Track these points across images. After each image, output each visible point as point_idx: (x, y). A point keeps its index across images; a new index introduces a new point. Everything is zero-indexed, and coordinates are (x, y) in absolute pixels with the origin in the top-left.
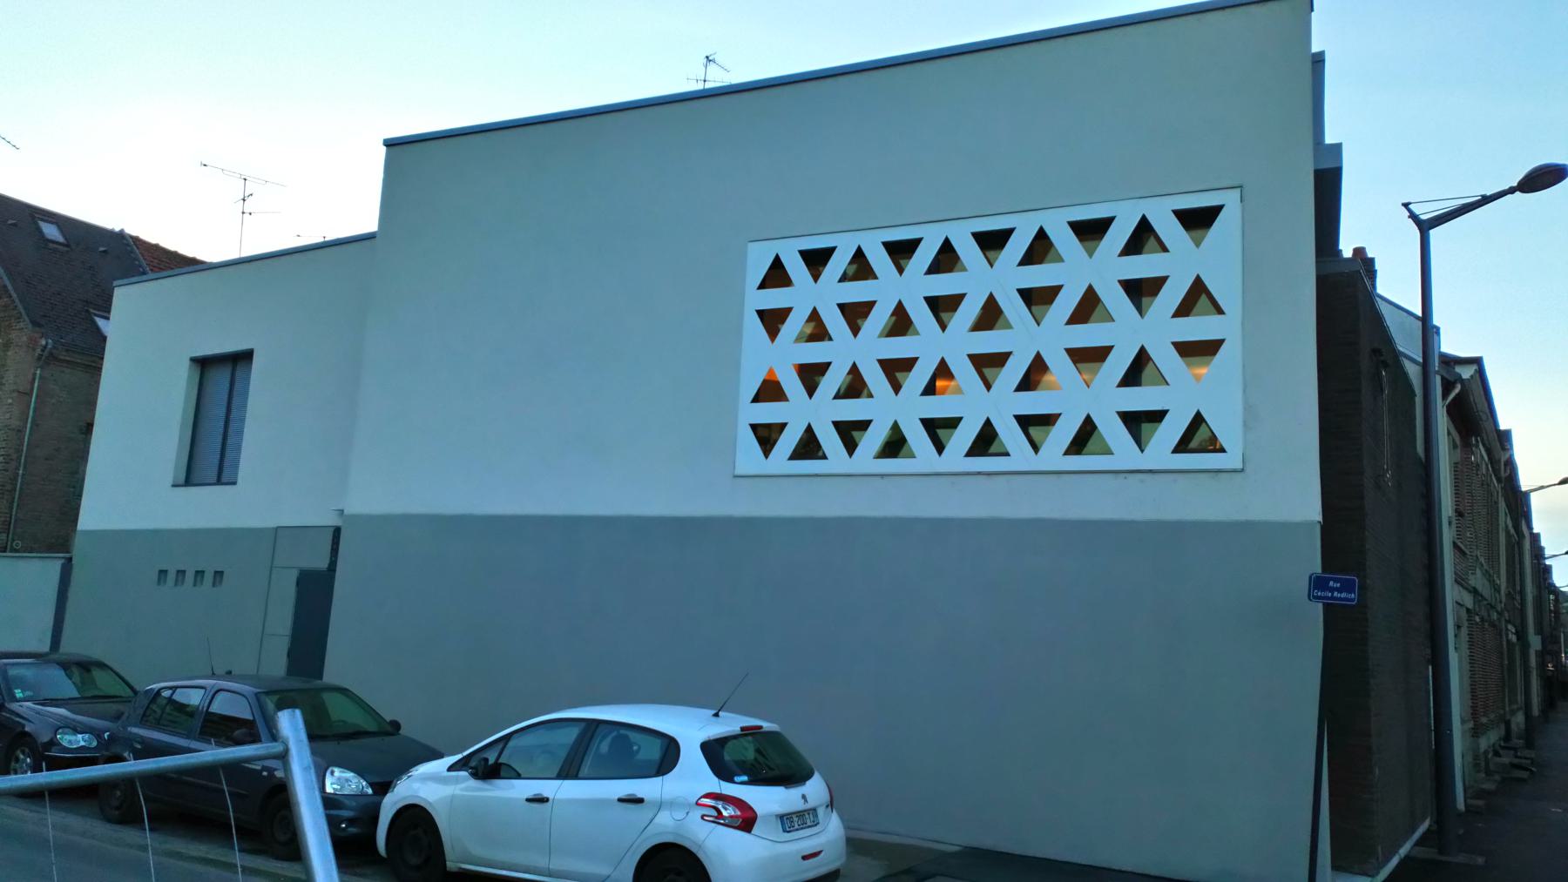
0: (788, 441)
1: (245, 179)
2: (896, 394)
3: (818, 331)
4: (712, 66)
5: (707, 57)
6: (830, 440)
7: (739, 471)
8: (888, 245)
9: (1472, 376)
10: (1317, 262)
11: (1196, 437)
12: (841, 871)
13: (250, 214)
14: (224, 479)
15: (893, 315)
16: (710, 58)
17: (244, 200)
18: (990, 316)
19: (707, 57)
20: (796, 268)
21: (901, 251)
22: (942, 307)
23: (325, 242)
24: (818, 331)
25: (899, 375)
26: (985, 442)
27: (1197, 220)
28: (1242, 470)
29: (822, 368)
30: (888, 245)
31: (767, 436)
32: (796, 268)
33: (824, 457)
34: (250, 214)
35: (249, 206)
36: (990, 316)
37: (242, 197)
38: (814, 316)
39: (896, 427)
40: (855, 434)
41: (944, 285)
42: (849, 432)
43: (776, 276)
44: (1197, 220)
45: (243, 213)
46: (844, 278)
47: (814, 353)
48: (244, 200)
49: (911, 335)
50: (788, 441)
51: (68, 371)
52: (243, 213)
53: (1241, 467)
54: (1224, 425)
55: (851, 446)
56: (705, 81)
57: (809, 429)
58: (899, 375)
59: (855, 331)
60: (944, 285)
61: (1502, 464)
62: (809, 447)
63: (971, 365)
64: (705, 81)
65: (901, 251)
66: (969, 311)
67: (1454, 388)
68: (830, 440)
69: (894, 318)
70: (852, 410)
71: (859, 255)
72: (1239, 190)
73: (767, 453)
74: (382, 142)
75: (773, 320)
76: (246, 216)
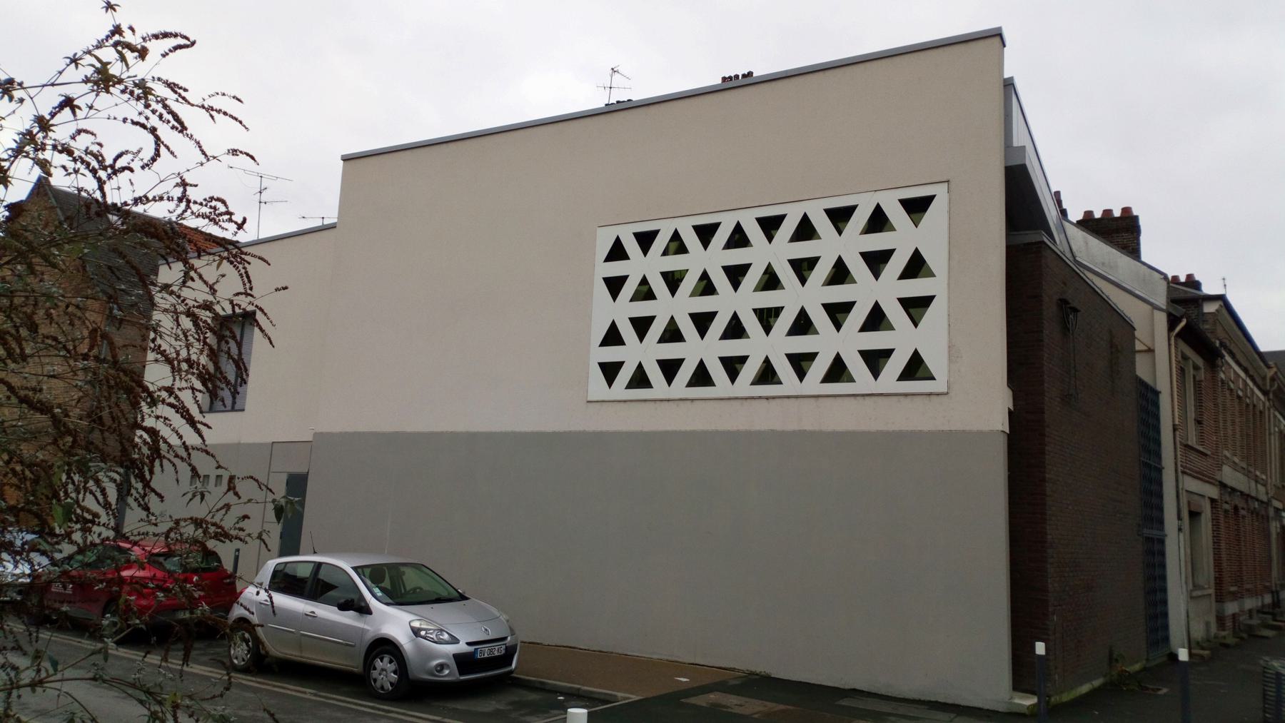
0: (625, 375)
1: (261, 177)
2: (702, 339)
3: (706, 287)
4: (616, 76)
5: (612, 69)
6: (784, 369)
7: (589, 399)
8: (761, 221)
9: (1217, 310)
10: (1008, 235)
11: (915, 368)
12: (371, 616)
13: (265, 203)
14: (236, 408)
15: (833, 267)
16: (615, 70)
17: (260, 192)
18: (840, 274)
19: (612, 69)
20: (631, 246)
21: (840, 217)
22: (876, 261)
23: (258, 240)
24: (706, 287)
25: (839, 316)
26: (767, 374)
27: (916, 207)
28: (947, 393)
29: (777, 311)
30: (761, 221)
31: (610, 370)
32: (631, 246)
33: (780, 383)
34: (265, 203)
35: (264, 197)
36: (840, 274)
37: (259, 190)
38: (705, 276)
39: (767, 361)
40: (804, 364)
41: (877, 242)
42: (800, 363)
43: (617, 253)
44: (916, 207)
45: (260, 202)
46: (665, 253)
47: (704, 304)
48: (260, 192)
49: (780, 289)
50: (625, 375)
51: (129, 327)
52: (260, 202)
53: (946, 391)
54: (932, 361)
55: (801, 374)
56: (611, 88)
57: (640, 366)
58: (839, 316)
59: (803, 281)
60: (877, 242)
61: (1268, 381)
62: (701, 377)
63: (882, 307)
64: (611, 88)
65: (840, 217)
66: (823, 270)
67: (1181, 321)
68: (784, 369)
69: (834, 270)
70: (801, 344)
71: (676, 236)
72: (946, 184)
73: (610, 384)
74: (340, 158)
75: (615, 285)
76: (263, 205)
